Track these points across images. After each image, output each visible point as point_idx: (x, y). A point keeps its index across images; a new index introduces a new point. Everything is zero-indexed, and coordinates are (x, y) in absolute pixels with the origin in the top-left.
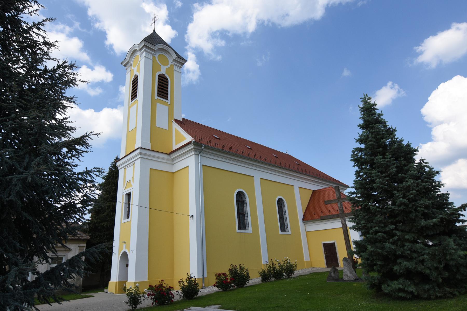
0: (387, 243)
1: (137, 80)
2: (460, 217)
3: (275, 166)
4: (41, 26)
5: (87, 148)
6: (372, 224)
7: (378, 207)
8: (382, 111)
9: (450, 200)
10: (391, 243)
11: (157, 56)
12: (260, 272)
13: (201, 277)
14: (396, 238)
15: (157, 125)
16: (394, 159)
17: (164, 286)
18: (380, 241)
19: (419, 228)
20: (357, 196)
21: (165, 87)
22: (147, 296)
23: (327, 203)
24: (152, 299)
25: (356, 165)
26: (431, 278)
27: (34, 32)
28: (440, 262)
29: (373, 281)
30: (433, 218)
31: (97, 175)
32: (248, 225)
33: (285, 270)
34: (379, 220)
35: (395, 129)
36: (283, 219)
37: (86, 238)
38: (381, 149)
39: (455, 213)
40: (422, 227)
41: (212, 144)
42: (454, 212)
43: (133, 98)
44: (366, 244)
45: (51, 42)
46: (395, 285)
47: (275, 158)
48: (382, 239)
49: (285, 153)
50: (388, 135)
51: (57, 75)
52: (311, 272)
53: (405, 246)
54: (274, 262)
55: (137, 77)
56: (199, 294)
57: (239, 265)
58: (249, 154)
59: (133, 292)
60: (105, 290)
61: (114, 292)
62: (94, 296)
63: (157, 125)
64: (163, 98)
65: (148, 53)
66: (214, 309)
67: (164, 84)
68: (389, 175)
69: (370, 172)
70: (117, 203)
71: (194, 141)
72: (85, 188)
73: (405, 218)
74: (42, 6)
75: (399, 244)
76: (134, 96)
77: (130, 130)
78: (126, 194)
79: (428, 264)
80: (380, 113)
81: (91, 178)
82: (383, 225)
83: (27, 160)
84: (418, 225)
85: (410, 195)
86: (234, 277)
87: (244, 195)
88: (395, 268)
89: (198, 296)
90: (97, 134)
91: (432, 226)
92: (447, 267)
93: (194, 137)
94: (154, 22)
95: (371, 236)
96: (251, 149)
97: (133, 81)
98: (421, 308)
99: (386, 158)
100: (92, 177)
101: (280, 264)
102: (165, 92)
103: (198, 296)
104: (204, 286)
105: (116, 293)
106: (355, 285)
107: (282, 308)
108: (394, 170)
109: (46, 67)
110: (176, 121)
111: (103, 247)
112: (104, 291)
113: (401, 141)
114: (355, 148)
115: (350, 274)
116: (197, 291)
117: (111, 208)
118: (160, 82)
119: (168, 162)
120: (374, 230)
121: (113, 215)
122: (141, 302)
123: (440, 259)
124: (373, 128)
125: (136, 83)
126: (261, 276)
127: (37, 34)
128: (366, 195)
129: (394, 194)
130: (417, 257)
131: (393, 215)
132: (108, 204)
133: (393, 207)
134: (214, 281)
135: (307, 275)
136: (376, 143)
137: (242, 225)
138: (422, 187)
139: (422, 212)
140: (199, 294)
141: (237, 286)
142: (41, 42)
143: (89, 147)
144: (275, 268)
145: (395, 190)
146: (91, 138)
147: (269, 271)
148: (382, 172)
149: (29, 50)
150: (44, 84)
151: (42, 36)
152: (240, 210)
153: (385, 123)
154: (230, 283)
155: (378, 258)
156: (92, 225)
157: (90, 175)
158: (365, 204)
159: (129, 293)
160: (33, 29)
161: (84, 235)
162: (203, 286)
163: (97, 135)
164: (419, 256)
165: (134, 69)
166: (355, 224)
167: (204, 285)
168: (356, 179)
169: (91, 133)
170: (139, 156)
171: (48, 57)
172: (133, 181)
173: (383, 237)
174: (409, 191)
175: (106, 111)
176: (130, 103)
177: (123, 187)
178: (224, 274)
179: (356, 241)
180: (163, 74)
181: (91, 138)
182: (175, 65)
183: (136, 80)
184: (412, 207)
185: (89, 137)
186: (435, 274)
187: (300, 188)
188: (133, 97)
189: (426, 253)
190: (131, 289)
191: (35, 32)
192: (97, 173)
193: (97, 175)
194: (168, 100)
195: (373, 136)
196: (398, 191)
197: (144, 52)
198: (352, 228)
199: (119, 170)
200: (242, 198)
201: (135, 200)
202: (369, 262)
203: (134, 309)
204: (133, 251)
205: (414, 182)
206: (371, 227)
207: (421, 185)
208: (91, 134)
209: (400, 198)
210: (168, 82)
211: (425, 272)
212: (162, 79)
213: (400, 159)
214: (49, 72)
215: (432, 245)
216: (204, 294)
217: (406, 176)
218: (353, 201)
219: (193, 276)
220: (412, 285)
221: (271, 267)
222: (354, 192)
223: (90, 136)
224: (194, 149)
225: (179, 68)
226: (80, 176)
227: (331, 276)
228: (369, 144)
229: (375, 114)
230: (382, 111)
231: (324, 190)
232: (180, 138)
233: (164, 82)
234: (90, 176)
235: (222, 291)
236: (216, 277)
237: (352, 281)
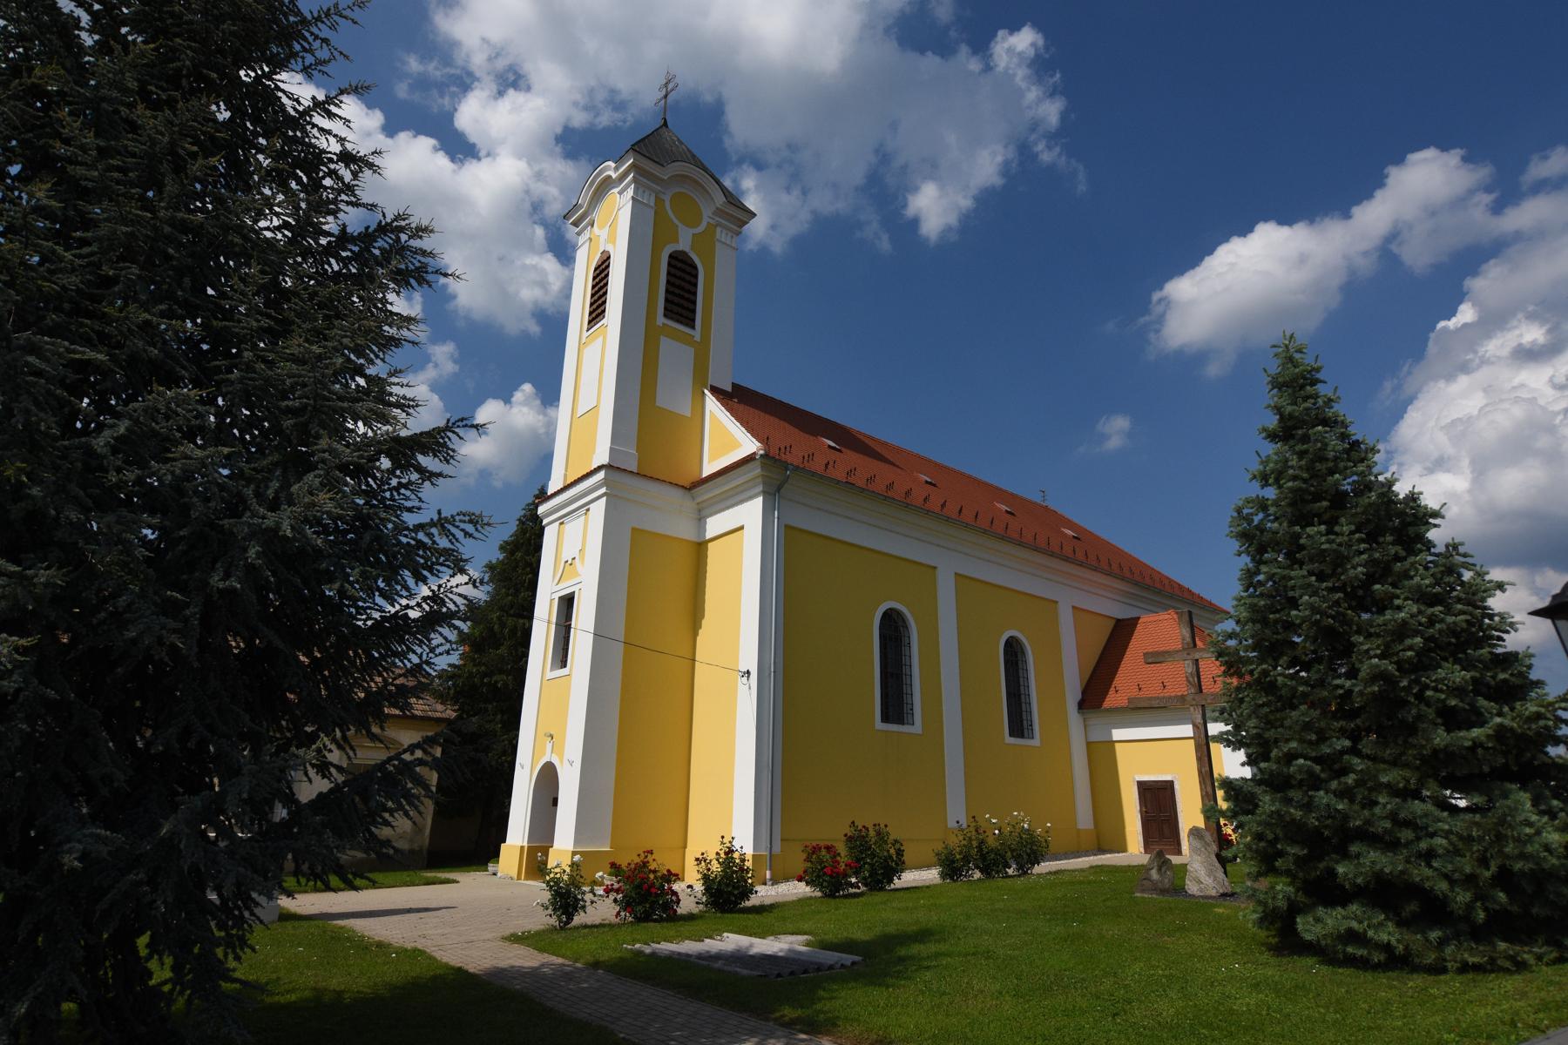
0: (1322, 793)
1: (608, 266)
2: (1560, 729)
4: (333, 109)
5: (448, 462)
7: (1305, 682)
8: (1336, 387)
9: (1534, 676)
10: (1334, 793)
11: (667, 199)
14: (1350, 779)
17: (652, 867)
18: (1301, 784)
19: (1425, 752)
22: (601, 892)
23: (1150, 660)
24: (615, 901)
27: (314, 126)
37: (444, 715)
38: (1325, 504)
40: (1435, 752)
42: (1543, 710)
43: (593, 319)
44: (1258, 790)
45: (361, 154)
47: (1008, 516)
51: (377, 252)
53: (1376, 803)
55: (609, 258)
56: (753, 901)
57: (875, 825)
59: (566, 878)
60: (491, 867)
62: (458, 882)
64: (681, 323)
67: (683, 280)
68: (1345, 585)
69: (1286, 572)
70: (536, 623)
71: (762, 452)
74: (341, 53)
76: (596, 312)
81: (450, 541)
83: (275, 485)
84: (1424, 743)
85: (1404, 650)
89: (748, 904)
91: (1468, 748)
96: (934, 485)
97: (596, 269)
98: (1410, 994)
99: (1337, 534)
100: (454, 536)
102: (686, 304)
105: (519, 878)
106: (1221, 911)
109: (344, 226)
113: (1390, 484)
115: (1207, 878)
116: (747, 892)
117: (519, 634)
118: (674, 276)
122: (584, 907)
123: (1486, 850)
124: (1305, 439)
125: (603, 275)
127: (321, 130)
129: (1353, 645)
130: (1412, 841)
131: (1345, 708)
133: (1348, 684)
134: (799, 863)
137: (895, 707)
138: (1445, 627)
139: (1440, 705)
140: (753, 901)
142: (335, 154)
143: (451, 461)
144: (982, 842)
145: (1358, 632)
146: (458, 435)
148: (1321, 577)
149: (301, 174)
150: (339, 273)
151: (335, 136)
157: (449, 530)
158: (1264, 670)
159: (552, 879)
160: (311, 116)
161: (440, 707)
164: (1418, 839)
165: (600, 232)
166: (1229, 728)
168: (1243, 594)
169: (462, 420)
170: (603, 490)
171: (354, 200)
172: (582, 559)
173: (1311, 773)
176: (585, 334)
179: (1227, 778)
180: (683, 253)
181: (458, 435)
182: (719, 224)
183: (603, 267)
184: (1408, 689)
185: (454, 432)
188: (594, 315)
189: (1442, 830)
190: (557, 870)
191: (317, 126)
192: (470, 528)
193: (467, 534)
194: (693, 327)
195: (1303, 463)
196: (1369, 636)
198: (1221, 738)
199: (542, 529)
205: (1420, 612)
206: (1276, 741)
207: (1442, 621)
208: (460, 424)
209: (1371, 658)
210: (696, 276)
213: (1381, 539)
214: (353, 239)
215: (1466, 809)
216: (767, 902)
217: (1398, 591)
218: (1226, 658)
219: (736, 844)
220: (1390, 924)
221: (970, 838)
223: (456, 430)
225: (730, 234)
228: (1288, 488)
234: (448, 534)
236: (804, 856)
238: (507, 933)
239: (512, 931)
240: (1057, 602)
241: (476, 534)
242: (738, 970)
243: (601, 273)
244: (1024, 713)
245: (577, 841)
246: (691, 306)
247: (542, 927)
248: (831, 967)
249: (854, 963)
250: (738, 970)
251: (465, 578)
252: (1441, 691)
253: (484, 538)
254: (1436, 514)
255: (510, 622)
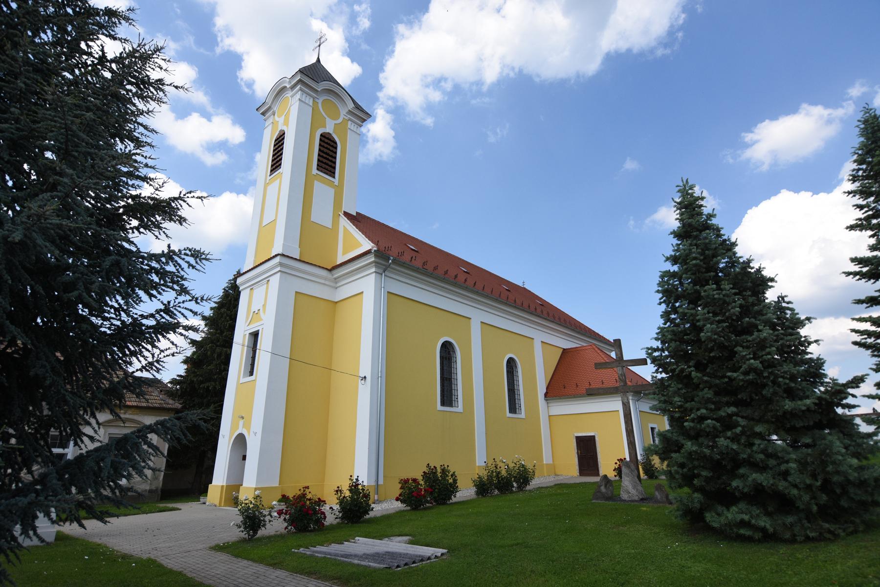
1: (284, 139)
3: (506, 303)
6: (693, 403)
8: (714, 209)
11: (320, 101)
12: (473, 479)
13: (373, 483)
14: (738, 430)
15: (313, 218)
16: (737, 291)
17: (308, 497)
18: (708, 435)
19: (778, 414)
20: (661, 354)
21: (332, 156)
22: (275, 514)
24: (285, 519)
25: (664, 300)
26: (799, 504)
28: (814, 476)
29: (690, 504)
30: (801, 399)
31: (190, 265)
32: (457, 399)
33: (515, 477)
34: (707, 397)
35: (736, 242)
36: (514, 392)
39: (843, 390)
40: (785, 413)
41: (406, 258)
43: (274, 169)
46: (734, 514)
47: (506, 291)
48: (712, 430)
49: (521, 285)
50: (725, 251)
52: (557, 483)
54: (498, 463)
55: (284, 134)
56: (372, 514)
57: (441, 466)
58: (466, 280)
59: (251, 506)
60: (202, 499)
61: (217, 503)
62: (180, 509)
63: (313, 218)
64: (327, 174)
65: (305, 95)
66: (400, 544)
67: (329, 149)
68: (727, 318)
71: (375, 249)
72: (164, 288)
73: (754, 395)
75: (743, 441)
77: (264, 223)
78: (250, 334)
79: (794, 478)
80: (711, 212)
81: (177, 270)
82: (713, 407)
84: (778, 408)
86: (431, 487)
87: (453, 348)
88: (735, 484)
89: (367, 516)
90: (202, 197)
91: (803, 411)
92: (826, 486)
93: (376, 243)
94: (319, 46)
95: (692, 424)
96: (468, 273)
97: (276, 140)
99: (722, 290)
100: (180, 266)
101: (508, 466)
103: (367, 516)
104: (377, 500)
105: (220, 505)
107: (526, 547)
108: (737, 311)
110: (346, 214)
111: (195, 417)
112: (200, 501)
114: (662, 270)
116: (367, 509)
117: (223, 357)
119: (327, 283)
120: (729, 413)
121: (225, 371)
122: (264, 525)
126: (475, 485)
128: (682, 353)
132: (218, 350)
134: (397, 490)
135: (551, 487)
136: (704, 263)
137: (447, 398)
139: (785, 386)
141: (435, 502)
144: (499, 473)
147: (490, 477)
148: (715, 314)
152: (445, 373)
153: (718, 230)
154: (424, 496)
155: (702, 464)
156: (185, 385)
157: (176, 261)
158: (682, 368)
161: (171, 401)
162: (376, 498)
163: (202, 200)
164: (779, 465)
165: (280, 120)
167: (378, 497)
170: (278, 269)
173: (714, 427)
174: (763, 348)
175: (228, 198)
176: (269, 178)
177: (246, 322)
178: (415, 480)
180: (329, 133)
182: (350, 120)
183: (281, 139)
185: (185, 201)
186: (806, 498)
187: (545, 345)
188: (274, 167)
192: (192, 260)
193: (190, 265)
194: (334, 177)
197: (298, 91)
199: (240, 292)
200: (449, 353)
201: (265, 343)
202: (685, 470)
203: (252, 537)
204: (255, 434)
206: (691, 410)
210: (336, 148)
211: (789, 494)
212: (326, 141)
216: (379, 515)
218: (659, 362)
222: (658, 347)
223: (186, 199)
224: (374, 264)
225: (356, 126)
226: (154, 264)
227: (600, 492)
229: (701, 214)
230: (714, 209)
231: (581, 349)
232: (350, 243)
233: (329, 147)
235: (411, 510)
236: (400, 486)
237: (636, 501)
238: (213, 544)
239: (216, 542)
240: (533, 339)
241: (198, 267)
242: (371, 564)
243: (279, 142)
244: (517, 400)
245: (258, 481)
246: (333, 165)
247: (238, 539)
248: (429, 558)
249: (442, 554)
250: (371, 564)
251: (188, 297)
252: (786, 378)
253: (202, 270)
254: (772, 280)
255: (218, 350)
